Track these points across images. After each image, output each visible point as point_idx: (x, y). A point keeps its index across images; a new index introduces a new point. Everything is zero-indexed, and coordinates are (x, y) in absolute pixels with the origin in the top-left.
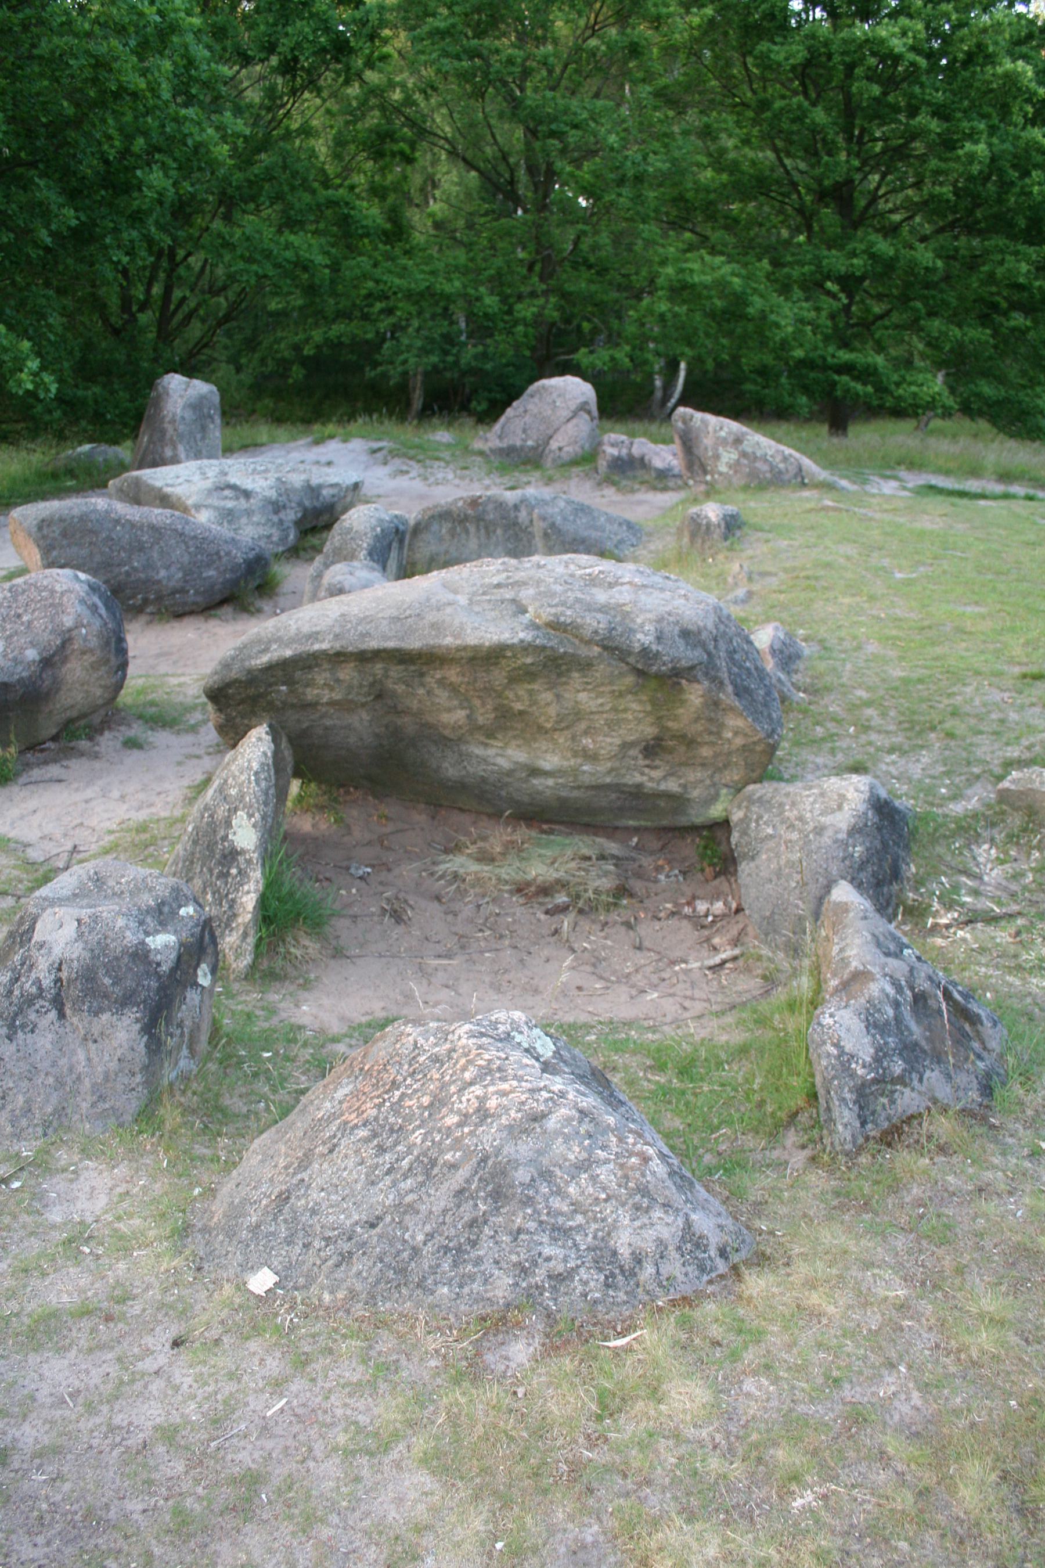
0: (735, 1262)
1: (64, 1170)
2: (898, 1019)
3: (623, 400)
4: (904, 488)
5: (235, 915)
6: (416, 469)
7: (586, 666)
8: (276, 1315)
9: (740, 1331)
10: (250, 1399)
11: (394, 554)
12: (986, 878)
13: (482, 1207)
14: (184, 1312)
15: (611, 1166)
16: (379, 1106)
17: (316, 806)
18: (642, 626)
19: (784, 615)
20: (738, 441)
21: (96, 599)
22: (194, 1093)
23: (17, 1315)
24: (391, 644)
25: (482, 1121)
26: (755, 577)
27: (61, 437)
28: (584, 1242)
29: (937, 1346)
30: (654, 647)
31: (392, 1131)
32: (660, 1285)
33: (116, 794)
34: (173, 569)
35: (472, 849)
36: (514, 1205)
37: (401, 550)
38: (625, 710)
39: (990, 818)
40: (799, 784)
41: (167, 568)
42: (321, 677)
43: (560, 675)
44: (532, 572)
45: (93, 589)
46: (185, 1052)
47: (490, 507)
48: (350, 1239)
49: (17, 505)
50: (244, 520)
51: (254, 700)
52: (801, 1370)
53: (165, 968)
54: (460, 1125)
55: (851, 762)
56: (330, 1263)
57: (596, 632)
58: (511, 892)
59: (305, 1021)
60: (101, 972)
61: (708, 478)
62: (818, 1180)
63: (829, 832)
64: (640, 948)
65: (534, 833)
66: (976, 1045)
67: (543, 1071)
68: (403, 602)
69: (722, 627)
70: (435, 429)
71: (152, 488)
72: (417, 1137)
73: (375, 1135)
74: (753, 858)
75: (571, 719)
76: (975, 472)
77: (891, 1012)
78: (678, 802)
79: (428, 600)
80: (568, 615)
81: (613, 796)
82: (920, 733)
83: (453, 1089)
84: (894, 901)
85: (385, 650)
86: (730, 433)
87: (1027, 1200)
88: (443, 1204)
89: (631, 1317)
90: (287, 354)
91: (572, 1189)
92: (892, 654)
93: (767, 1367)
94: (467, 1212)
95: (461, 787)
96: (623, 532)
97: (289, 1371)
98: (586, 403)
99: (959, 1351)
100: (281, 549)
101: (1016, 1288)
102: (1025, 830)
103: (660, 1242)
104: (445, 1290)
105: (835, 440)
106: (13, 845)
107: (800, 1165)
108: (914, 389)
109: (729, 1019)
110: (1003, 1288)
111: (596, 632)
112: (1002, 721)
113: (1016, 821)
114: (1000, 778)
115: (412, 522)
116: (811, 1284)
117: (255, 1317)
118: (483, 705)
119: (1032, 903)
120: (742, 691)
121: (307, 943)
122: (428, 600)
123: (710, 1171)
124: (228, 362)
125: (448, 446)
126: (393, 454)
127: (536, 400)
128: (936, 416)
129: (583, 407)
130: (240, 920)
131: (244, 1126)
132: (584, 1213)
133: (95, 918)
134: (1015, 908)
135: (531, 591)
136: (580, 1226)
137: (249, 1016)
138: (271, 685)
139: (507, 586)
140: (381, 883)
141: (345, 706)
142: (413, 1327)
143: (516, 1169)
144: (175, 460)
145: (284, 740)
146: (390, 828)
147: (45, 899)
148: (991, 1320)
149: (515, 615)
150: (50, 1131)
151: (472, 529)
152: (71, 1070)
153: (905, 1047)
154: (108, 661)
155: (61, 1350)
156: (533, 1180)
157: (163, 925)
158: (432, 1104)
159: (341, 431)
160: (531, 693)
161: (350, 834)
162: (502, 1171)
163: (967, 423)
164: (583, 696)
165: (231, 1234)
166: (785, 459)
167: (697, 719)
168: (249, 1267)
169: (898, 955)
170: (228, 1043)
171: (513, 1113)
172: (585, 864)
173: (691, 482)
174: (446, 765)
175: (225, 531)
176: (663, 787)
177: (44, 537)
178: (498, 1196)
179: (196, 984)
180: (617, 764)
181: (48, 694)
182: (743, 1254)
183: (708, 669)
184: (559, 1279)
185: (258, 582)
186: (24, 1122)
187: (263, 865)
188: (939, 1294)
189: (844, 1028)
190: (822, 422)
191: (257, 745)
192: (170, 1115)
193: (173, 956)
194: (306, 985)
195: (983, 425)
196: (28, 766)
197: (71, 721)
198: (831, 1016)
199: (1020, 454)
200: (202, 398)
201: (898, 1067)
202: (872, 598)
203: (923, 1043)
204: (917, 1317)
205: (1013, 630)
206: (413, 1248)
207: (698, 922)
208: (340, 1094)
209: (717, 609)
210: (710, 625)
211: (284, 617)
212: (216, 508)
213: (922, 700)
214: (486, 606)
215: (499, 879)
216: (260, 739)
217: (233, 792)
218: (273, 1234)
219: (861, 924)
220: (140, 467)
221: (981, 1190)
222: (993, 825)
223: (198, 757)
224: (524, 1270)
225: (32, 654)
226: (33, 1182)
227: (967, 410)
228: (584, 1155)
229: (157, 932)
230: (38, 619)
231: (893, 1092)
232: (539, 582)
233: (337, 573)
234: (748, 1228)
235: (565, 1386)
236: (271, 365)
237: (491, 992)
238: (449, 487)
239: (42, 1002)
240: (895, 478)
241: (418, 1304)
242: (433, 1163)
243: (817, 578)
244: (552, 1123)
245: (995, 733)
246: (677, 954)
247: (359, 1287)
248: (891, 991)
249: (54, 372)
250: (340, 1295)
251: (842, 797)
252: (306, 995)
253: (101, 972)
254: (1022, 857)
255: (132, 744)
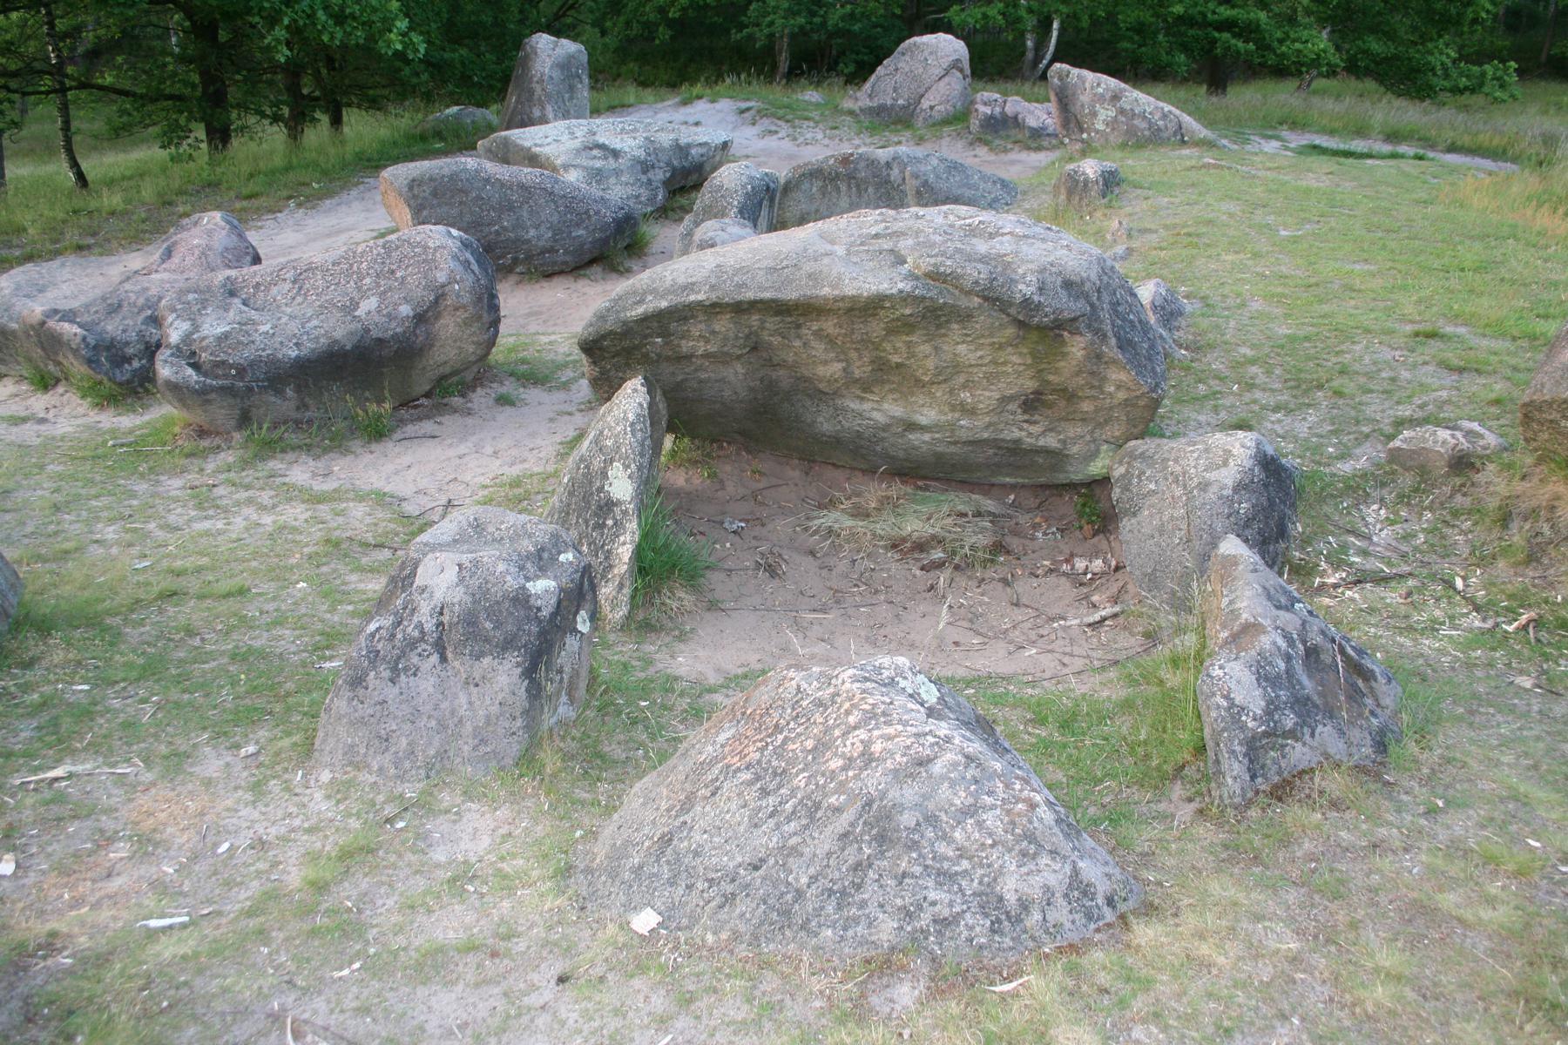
0: (1122, 911)
1: (447, 812)
2: (1289, 672)
3: (994, 60)
4: (1287, 149)
5: (611, 567)
6: (785, 129)
7: (965, 317)
8: (660, 954)
9: (1128, 980)
10: (636, 1035)
11: (764, 212)
12: (1375, 539)
13: (867, 851)
14: (568, 949)
15: (998, 812)
16: (762, 750)
17: (689, 460)
18: (1024, 276)
19: (1165, 272)
20: (1116, 98)
21: (468, 255)
22: (573, 739)
23: (405, 949)
24: (767, 295)
25: (866, 766)
26: (1135, 233)
27: (428, 98)
28: (970, 887)
29: (1331, 1000)
30: (1036, 298)
31: (775, 774)
32: (1047, 932)
33: (489, 450)
34: (543, 229)
35: (847, 504)
36: (899, 849)
37: (769, 206)
38: (1005, 363)
39: (1380, 478)
40: (1183, 440)
41: (537, 227)
42: (696, 329)
43: (939, 327)
44: (911, 222)
45: (465, 245)
46: (564, 698)
47: (862, 164)
48: (733, 881)
49: (386, 167)
50: (612, 180)
51: (628, 353)
52: (1190, 1019)
53: (545, 613)
54: (845, 768)
55: (1234, 420)
56: (713, 904)
57: (977, 282)
58: (885, 547)
59: (682, 671)
60: (483, 615)
61: (1085, 136)
62: (1206, 833)
63: (1214, 488)
64: (1017, 605)
65: (909, 490)
66: (1369, 701)
67: (928, 716)
68: (780, 252)
69: (1105, 278)
70: (804, 89)
71: (522, 148)
72: (800, 780)
73: (758, 778)
74: (1134, 514)
75: (949, 372)
76: (1361, 132)
77: (1282, 666)
78: (1057, 458)
79: (805, 250)
80: (948, 265)
81: (991, 452)
82: (1306, 392)
83: (837, 733)
84: (1280, 559)
85: (761, 301)
86: (1107, 89)
87: (1424, 858)
88: (827, 847)
89: (1017, 963)
90: (652, 17)
91: (957, 835)
92: (1278, 311)
93: (1156, 1015)
94: (851, 855)
95: (836, 442)
96: (998, 191)
97: (674, 1009)
98: (958, 60)
99: (1354, 1005)
100: (649, 209)
101: (1413, 943)
102: (1416, 490)
103: (1047, 889)
104: (829, 932)
105: (1214, 99)
106: (388, 499)
107: (1188, 818)
108: (1298, 45)
109: (1112, 674)
110: (1400, 944)
111: (977, 282)
112: (1393, 380)
113: (1407, 480)
114: (1391, 437)
115: (782, 181)
116: (1201, 936)
117: (639, 956)
118: (860, 357)
119: (1424, 564)
120: (1125, 344)
121: (683, 595)
122: (805, 250)
123: (1095, 822)
124: (593, 25)
125: (817, 105)
126: (762, 114)
127: (907, 58)
128: (1320, 75)
129: (956, 65)
130: (616, 571)
131: (626, 771)
132: (970, 858)
133: (476, 563)
134: (1406, 569)
135: (910, 242)
136: (966, 871)
137: (625, 666)
138: (646, 337)
139: (885, 236)
140: (755, 538)
141: (721, 358)
142: (797, 968)
143: (901, 813)
144: (543, 121)
145: (659, 392)
146: (764, 483)
147: (426, 545)
148: (1387, 975)
149: (893, 265)
150: (432, 774)
151: (843, 188)
152: (453, 712)
153: (1297, 701)
154: (481, 317)
155: (449, 984)
156: (918, 824)
157: (543, 571)
158: (815, 748)
159: (708, 91)
160: (909, 345)
161: (723, 488)
162: (887, 815)
163: (1353, 83)
164: (962, 348)
165: (613, 875)
166: (1165, 116)
167: (1078, 374)
168: (632, 907)
169: (1289, 608)
170: (605, 691)
171: (898, 758)
172: (960, 521)
173: (1067, 141)
174: (820, 419)
175: (595, 191)
176: (1041, 443)
177: (414, 197)
178: (882, 839)
179: (576, 631)
180: (995, 419)
181: (421, 350)
182: (1131, 904)
183: (1091, 320)
184: (943, 923)
185: (627, 241)
186: (407, 764)
187: (639, 517)
188: (1333, 949)
189: (1235, 681)
190: (1200, 83)
191: (632, 397)
192: (550, 760)
193: (554, 601)
194: (682, 637)
195: (1370, 84)
196: (402, 422)
197: (444, 378)
198: (1221, 667)
199: (1409, 113)
200: (571, 57)
201: (1289, 721)
202: (1256, 255)
203: (1315, 698)
204: (1310, 970)
205: (1404, 288)
206: (797, 891)
207: (1077, 580)
208: (722, 738)
209: (1101, 261)
210: (1094, 277)
211: (659, 268)
212: (585, 168)
213: (1309, 358)
214: (864, 256)
215: (874, 535)
216: (635, 390)
217: (609, 443)
218: (655, 875)
219: (1252, 576)
220: (508, 128)
221: (1375, 846)
222: (1383, 485)
223: (570, 414)
224: (909, 915)
225: (405, 310)
226: (417, 822)
227: (1353, 68)
228: (971, 800)
229: (538, 577)
230: (412, 274)
231: (1283, 746)
232: (918, 233)
233: (709, 229)
234: (1135, 878)
235: (951, 1028)
236: (636, 30)
237: (867, 646)
238: (818, 146)
239: (424, 646)
240: (1277, 138)
241: (802, 946)
242: (817, 806)
243: (1198, 235)
244: (937, 768)
245: (1385, 392)
246: (1055, 610)
247: (742, 928)
248: (1282, 644)
249: (421, 33)
250: (724, 936)
251: (1228, 453)
252: (682, 646)
253: (483, 615)
254: (1414, 517)
255: (504, 401)
